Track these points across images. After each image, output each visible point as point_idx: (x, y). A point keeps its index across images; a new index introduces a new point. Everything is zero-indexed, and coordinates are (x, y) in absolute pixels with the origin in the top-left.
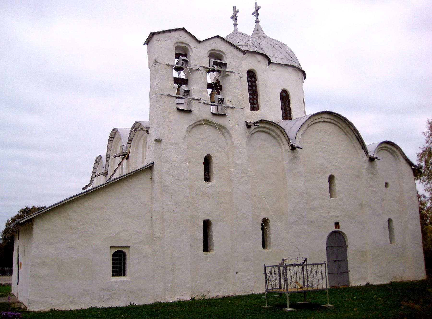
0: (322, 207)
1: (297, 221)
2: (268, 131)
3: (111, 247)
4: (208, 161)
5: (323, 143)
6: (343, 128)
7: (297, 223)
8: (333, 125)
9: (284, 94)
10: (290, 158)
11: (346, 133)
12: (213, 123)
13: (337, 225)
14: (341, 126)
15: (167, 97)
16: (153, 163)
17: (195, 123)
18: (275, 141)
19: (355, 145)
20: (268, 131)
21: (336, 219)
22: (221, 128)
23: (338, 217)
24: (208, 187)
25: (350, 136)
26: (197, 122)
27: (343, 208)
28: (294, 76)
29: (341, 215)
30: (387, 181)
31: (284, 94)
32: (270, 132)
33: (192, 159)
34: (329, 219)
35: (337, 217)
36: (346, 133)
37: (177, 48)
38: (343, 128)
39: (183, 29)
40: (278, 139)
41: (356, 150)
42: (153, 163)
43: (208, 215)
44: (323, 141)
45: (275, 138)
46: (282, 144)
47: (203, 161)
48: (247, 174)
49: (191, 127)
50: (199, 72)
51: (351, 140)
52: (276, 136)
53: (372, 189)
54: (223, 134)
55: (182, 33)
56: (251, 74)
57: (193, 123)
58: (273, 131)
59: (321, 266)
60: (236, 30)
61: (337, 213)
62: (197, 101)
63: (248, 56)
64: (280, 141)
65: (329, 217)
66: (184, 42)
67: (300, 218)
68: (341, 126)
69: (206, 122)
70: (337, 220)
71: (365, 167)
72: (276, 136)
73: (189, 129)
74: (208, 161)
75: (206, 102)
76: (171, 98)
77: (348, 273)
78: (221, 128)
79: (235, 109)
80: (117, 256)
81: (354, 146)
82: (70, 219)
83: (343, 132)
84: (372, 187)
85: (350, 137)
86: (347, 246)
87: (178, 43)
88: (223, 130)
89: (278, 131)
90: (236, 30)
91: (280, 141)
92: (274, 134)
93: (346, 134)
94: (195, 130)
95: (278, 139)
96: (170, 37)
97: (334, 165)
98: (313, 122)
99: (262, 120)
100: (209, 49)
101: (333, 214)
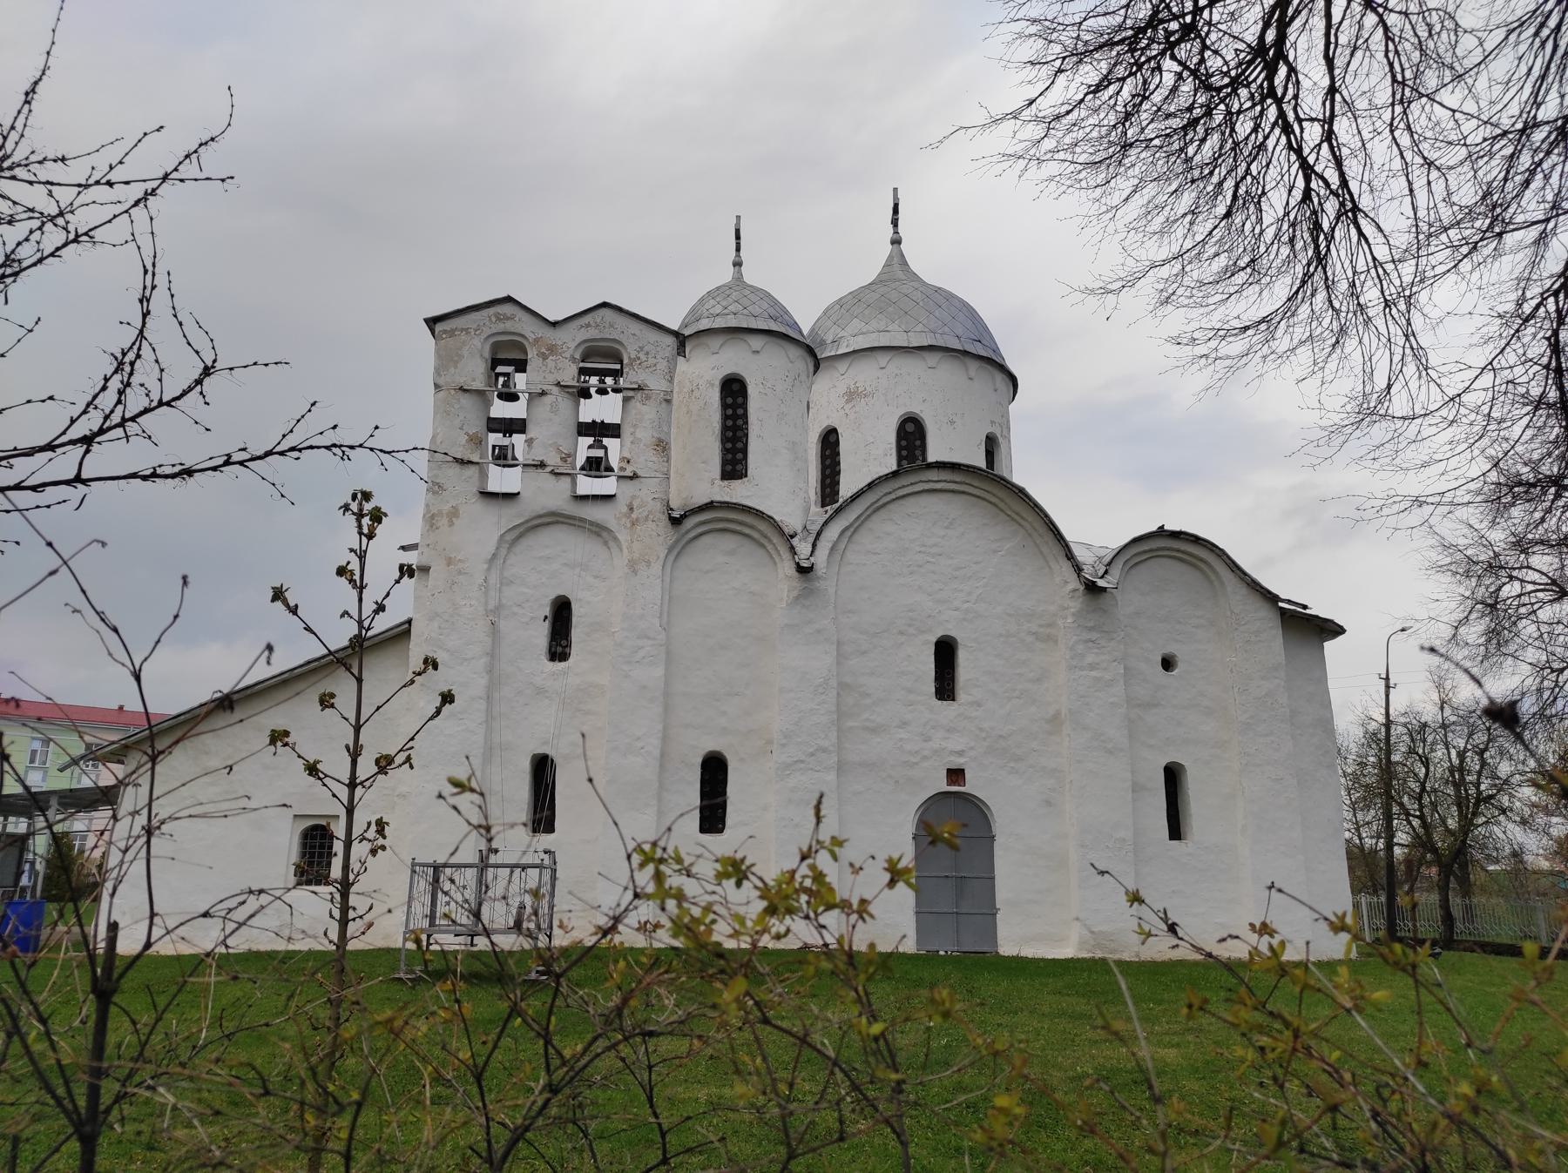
1: (802, 762)
2: (739, 528)
5: (923, 549)
6: (1001, 505)
7: (802, 765)
9: (910, 427)
10: (795, 593)
11: (1013, 515)
13: (956, 775)
14: (993, 500)
16: (409, 622)
17: (527, 522)
18: (761, 552)
19: (1045, 550)
20: (739, 528)
21: (952, 758)
22: (598, 530)
23: (961, 753)
27: (981, 730)
28: (984, 383)
29: (972, 748)
30: (1171, 649)
31: (910, 427)
32: (747, 531)
33: (515, 609)
34: (925, 758)
36: (1013, 515)
37: (496, 347)
38: (1001, 505)
39: (605, 305)
40: (769, 547)
41: (1047, 562)
42: (409, 622)
43: (546, 743)
45: (763, 546)
46: (777, 560)
47: (547, 611)
48: (654, 639)
49: (517, 532)
51: (1030, 535)
52: (763, 541)
53: (1093, 673)
54: (606, 543)
56: (735, 387)
58: (752, 527)
61: (957, 743)
64: (773, 552)
65: (926, 753)
67: (812, 755)
68: (993, 500)
69: (553, 519)
70: (957, 762)
72: (763, 541)
73: (509, 538)
77: (994, 915)
78: (598, 530)
80: (313, 838)
81: (1041, 553)
82: (207, 753)
84: (1092, 667)
87: (494, 335)
88: (605, 534)
89: (763, 526)
90: (739, 278)
91: (773, 552)
92: (756, 535)
93: (1013, 519)
95: (769, 547)
98: (893, 496)
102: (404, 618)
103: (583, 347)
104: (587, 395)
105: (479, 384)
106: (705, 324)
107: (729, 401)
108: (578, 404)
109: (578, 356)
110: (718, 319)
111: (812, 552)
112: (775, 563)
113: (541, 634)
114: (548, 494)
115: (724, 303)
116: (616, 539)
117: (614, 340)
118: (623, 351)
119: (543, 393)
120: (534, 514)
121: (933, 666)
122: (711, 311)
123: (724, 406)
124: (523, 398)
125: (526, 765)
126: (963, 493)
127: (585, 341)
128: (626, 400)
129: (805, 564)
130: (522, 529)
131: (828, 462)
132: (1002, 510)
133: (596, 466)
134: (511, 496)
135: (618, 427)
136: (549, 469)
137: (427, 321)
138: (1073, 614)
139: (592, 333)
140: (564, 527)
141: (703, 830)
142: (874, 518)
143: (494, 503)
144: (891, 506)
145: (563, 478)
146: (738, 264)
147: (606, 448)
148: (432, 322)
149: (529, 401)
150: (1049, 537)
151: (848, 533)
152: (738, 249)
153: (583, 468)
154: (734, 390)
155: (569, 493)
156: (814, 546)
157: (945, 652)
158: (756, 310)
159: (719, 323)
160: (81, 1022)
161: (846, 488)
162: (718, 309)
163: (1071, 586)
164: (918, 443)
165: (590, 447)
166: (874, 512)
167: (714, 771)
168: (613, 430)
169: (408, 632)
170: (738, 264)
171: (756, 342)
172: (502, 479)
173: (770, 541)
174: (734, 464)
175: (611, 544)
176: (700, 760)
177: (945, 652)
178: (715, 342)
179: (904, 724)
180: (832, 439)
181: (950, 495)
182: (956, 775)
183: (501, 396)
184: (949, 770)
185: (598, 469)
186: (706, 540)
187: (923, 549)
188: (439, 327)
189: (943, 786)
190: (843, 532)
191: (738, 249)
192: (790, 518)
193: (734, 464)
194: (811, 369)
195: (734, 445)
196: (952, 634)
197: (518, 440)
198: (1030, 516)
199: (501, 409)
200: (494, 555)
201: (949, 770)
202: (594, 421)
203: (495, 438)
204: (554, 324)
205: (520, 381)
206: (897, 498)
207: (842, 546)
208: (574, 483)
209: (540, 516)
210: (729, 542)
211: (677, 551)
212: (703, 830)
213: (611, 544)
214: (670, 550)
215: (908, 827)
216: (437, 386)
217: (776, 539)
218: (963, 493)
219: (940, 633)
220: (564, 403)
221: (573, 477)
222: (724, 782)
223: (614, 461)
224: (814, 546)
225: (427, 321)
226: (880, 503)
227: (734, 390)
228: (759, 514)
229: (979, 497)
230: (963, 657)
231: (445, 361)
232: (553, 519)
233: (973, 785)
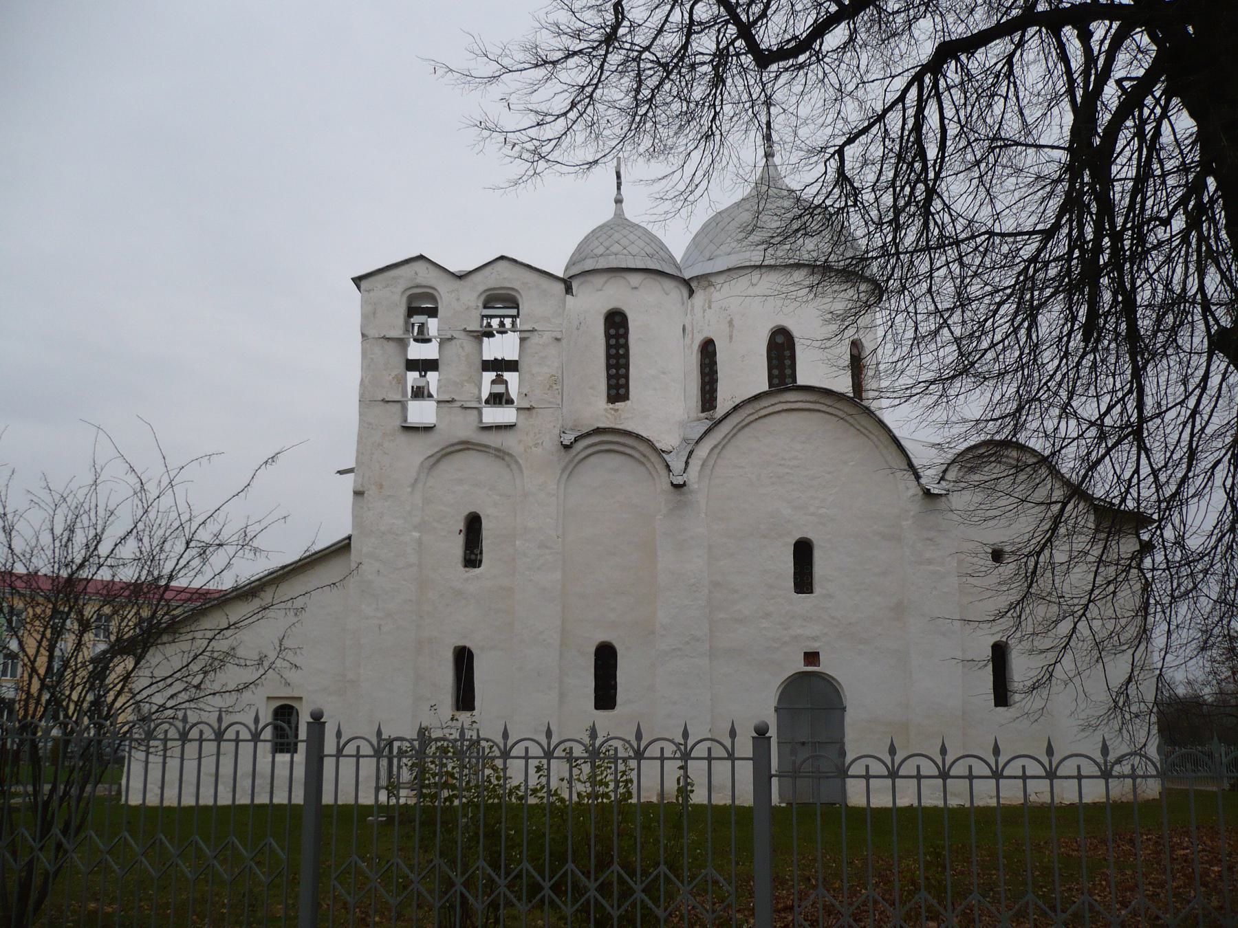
0: (767, 615)
1: (679, 649)
3: (269, 698)
4: (473, 525)
5: (783, 462)
8: (823, 414)
9: (780, 339)
12: (485, 446)
13: (812, 657)
15: (382, 403)
17: (443, 449)
22: (501, 454)
23: (815, 639)
24: (467, 579)
25: (871, 436)
26: (447, 447)
35: (813, 638)
37: (411, 298)
42: (349, 538)
44: (783, 459)
45: (642, 463)
47: (461, 525)
49: (433, 460)
50: (453, 342)
51: (877, 447)
52: (642, 459)
53: (931, 568)
54: (509, 466)
55: (419, 267)
56: (617, 319)
57: (436, 450)
58: (633, 448)
59: (363, 756)
60: (619, 214)
62: (448, 405)
63: (606, 282)
64: (652, 470)
66: (424, 284)
69: (465, 446)
70: (812, 646)
71: (912, 513)
72: (642, 459)
73: (427, 464)
74: (473, 525)
75: (469, 405)
76: (388, 406)
78: (501, 454)
79: (534, 411)
83: (852, 430)
84: (930, 562)
85: (875, 439)
86: (844, 709)
88: (507, 458)
89: (643, 447)
90: (619, 214)
91: (652, 470)
93: (861, 432)
94: (444, 465)
96: (394, 278)
97: (812, 514)
98: (756, 416)
99: (598, 428)
100: (481, 288)
101: (799, 631)
102: (345, 535)
103: (488, 293)
104: (490, 335)
105: (397, 333)
106: (589, 265)
107: (612, 332)
108: (481, 342)
109: (481, 305)
110: (601, 260)
111: (685, 469)
112: (653, 478)
113: (457, 546)
114: (461, 427)
115: (606, 244)
116: (517, 462)
117: (513, 289)
118: (518, 297)
119: (452, 339)
120: (448, 444)
121: (792, 564)
122: (595, 251)
123: (608, 337)
124: (435, 344)
125: (449, 657)
126: (819, 411)
127: (485, 291)
128: (522, 340)
129: (679, 481)
130: (439, 455)
131: (707, 379)
132: (852, 425)
133: (498, 399)
134: (428, 429)
135: (516, 362)
136: (459, 404)
137: (353, 279)
138: (913, 516)
139: (492, 283)
140: (471, 452)
141: (597, 707)
142: (740, 435)
143: (412, 435)
144: (753, 425)
145: (469, 411)
146: (619, 201)
147: (506, 383)
148: (358, 281)
149: (441, 344)
150: (893, 448)
151: (716, 451)
152: (619, 188)
153: (487, 402)
154: (616, 323)
155: (476, 424)
156: (687, 463)
157: (803, 552)
158: (634, 249)
159: (602, 264)
160: (631, 781)
161: (724, 401)
162: (601, 250)
163: (911, 492)
164: (787, 353)
165: (493, 382)
166: (739, 430)
167: (606, 658)
168: (512, 366)
169: (349, 545)
170: (619, 201)
171: (635, 279)
172: (421, 412)
173: (649, 460)
174: (618, 390)
175: (514, 466)
176: (593, 649)
177: (803, 552)
178: (599, 280)
179: (767, 615)
180: (710, 349)
181: (806, 413)
182: (812, 657)
183: (416, 340)
184: (805, 653)
185: (500, 403)
186: (593, 459)
187: (783, 462)
188: (364, 284)
189: (801, 667)
190: (712, 449)
191: (619, 188)
192: (667, 439)
193: (618, 390)
194: (685, 293)
195: (617, 371)
196: (809, 536)
197: (432, 376)
198: (876, 430)
199: (417, 351)
200: (416, 480)
201: (805, 653)
202: (496, 359)
203: (412, 376)
204: (461, 277)
205: (433, 325)
206: (760, 418)
207: (711, 462)
208: (480, 414)
209: (453, 445)
210: (614, 461)
211: (570, 470)
212: (597, 707)
213: (514, 466)
214: (563, 471)
215: (772, 700)
216: (363, 335)
217: (654, 458)
218: (819, 411)
219: (797, 536)
220: (468, 344)
221: (479, 410)
222: (614, 667)
223: (514, 393)
224: (687, 463)
225: (353, 279)
226: (744, 423)
227: (616, 323)
228: (638, 437)
229: (832, 414)
230: (818, 555)
231: (368, 317)
232: (465, 446)
233: (826, 666)
